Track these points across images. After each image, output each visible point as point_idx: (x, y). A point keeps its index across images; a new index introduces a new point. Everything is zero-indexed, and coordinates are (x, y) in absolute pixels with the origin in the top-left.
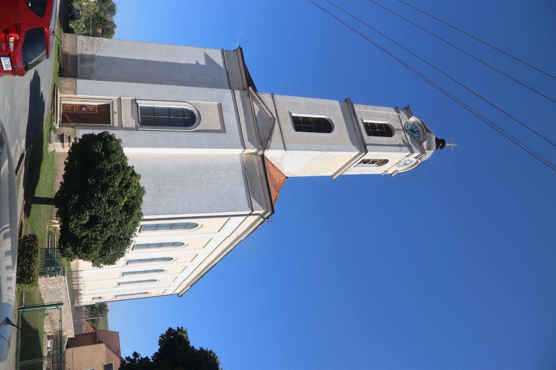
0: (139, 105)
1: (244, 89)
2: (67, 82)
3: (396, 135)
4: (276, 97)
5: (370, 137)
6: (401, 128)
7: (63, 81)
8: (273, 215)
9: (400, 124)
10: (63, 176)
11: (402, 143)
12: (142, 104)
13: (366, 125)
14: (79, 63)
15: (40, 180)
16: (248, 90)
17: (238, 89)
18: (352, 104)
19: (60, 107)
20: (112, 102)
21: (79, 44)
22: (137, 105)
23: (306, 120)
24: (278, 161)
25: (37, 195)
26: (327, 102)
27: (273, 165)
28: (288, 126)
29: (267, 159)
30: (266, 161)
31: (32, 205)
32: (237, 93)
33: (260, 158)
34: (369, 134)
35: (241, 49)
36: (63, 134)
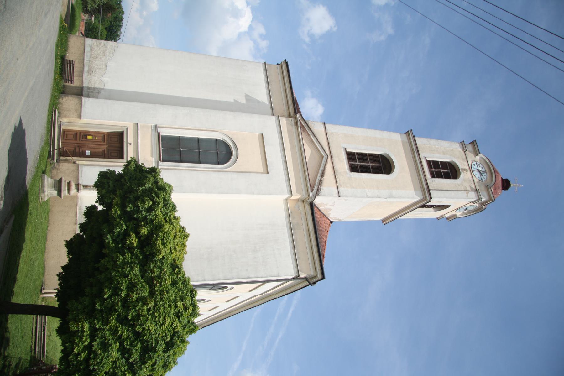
0: (161, 134)
1: (290, 116)
2: (68, 102)
3: (462, 175)
4: (327, 126)
5: (434, 179)
6: (467, 168)
7: (64, 99)
8: (323, 280)
9: (466, 163)
10: (59, 275)
11: (469, 189)
12: (165, 132)
13: (429, 162)
14: (85, 75)
15: (28, 151)
16: (296, 118)
17: (283, 116)
18: (414, 137)
19: (59, 135)
20: (127, 129)
21: (87, 49)
22: (159, 134)
23: (363, 157)
24: (327, 207)
25: (18, 299)
26: (385, 135)
27: (320, 210)
28: (343, 164)
29: (315, 205)
30: (315, 209)
31: (10, 316)
32: (284, 121)
33: (308, 207)
34: (433, 175)
35: (287, 63)
36: (61, 179)
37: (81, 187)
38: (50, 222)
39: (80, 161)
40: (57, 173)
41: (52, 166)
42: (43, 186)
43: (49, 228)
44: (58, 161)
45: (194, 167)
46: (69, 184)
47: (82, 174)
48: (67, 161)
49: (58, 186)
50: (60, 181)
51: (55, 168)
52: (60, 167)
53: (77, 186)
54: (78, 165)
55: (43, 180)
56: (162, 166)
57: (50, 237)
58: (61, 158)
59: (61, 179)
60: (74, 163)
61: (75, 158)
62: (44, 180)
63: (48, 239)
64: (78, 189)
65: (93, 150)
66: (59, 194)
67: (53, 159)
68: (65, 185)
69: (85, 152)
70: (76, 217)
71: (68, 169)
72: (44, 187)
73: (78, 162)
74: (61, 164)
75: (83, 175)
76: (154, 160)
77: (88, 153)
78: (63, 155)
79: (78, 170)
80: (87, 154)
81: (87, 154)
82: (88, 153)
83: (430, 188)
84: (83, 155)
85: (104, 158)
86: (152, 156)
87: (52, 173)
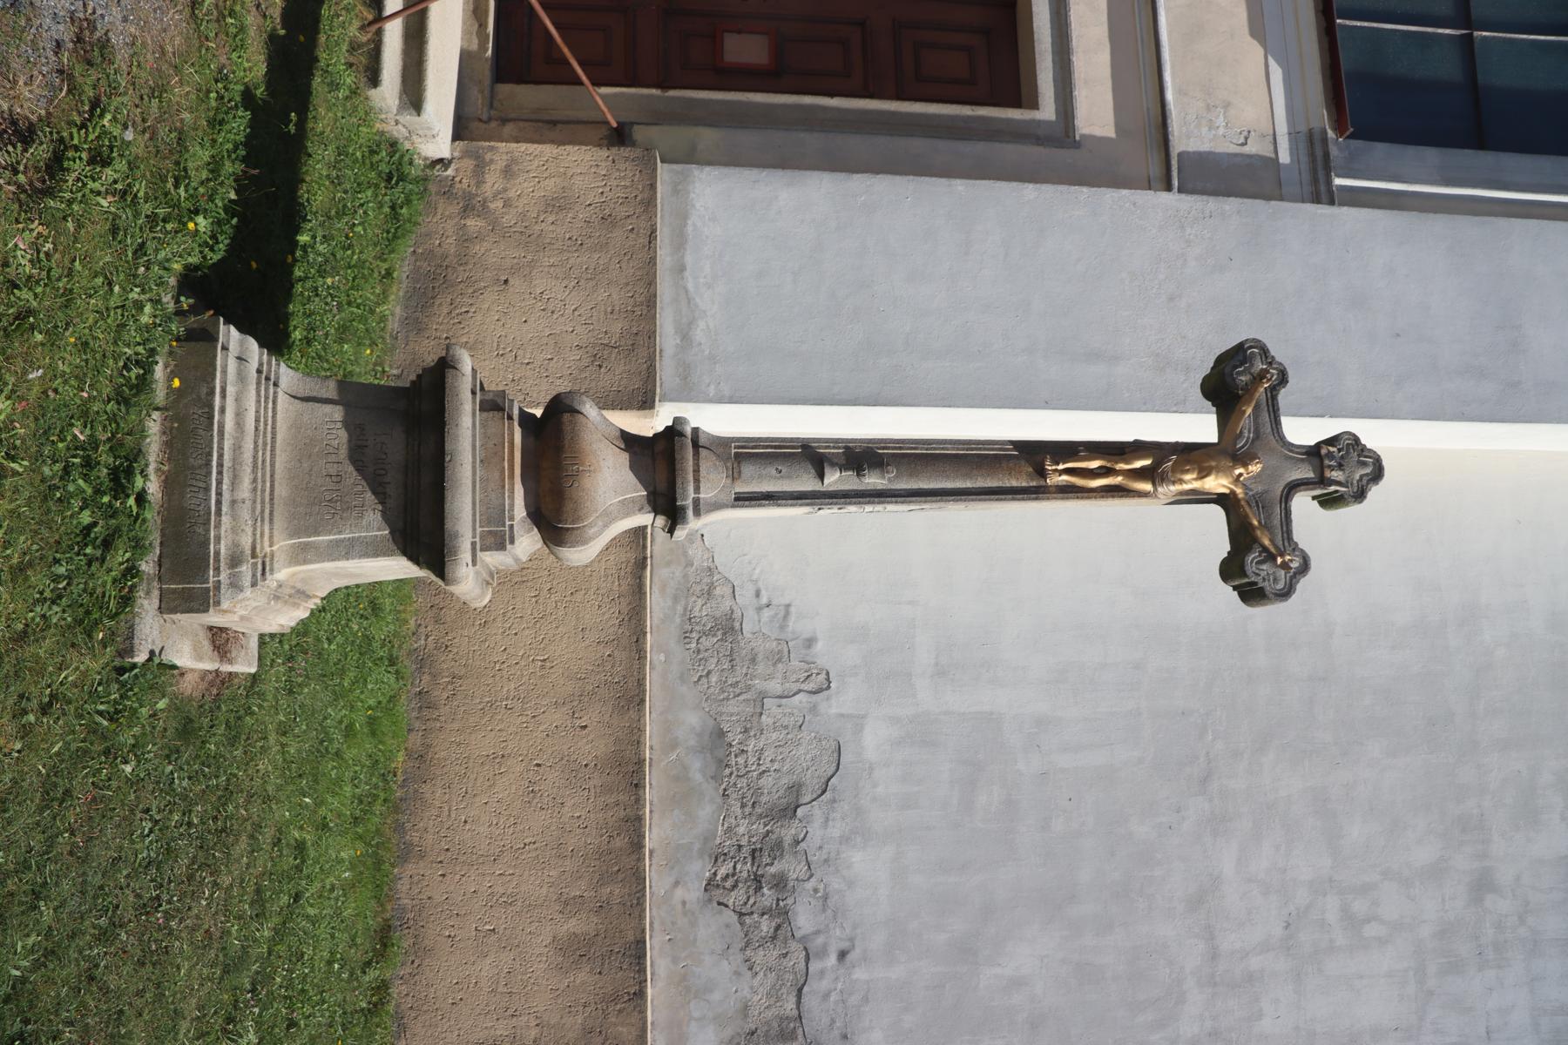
53: (662, 463)
68: (490, 457)
71: (557, 204)
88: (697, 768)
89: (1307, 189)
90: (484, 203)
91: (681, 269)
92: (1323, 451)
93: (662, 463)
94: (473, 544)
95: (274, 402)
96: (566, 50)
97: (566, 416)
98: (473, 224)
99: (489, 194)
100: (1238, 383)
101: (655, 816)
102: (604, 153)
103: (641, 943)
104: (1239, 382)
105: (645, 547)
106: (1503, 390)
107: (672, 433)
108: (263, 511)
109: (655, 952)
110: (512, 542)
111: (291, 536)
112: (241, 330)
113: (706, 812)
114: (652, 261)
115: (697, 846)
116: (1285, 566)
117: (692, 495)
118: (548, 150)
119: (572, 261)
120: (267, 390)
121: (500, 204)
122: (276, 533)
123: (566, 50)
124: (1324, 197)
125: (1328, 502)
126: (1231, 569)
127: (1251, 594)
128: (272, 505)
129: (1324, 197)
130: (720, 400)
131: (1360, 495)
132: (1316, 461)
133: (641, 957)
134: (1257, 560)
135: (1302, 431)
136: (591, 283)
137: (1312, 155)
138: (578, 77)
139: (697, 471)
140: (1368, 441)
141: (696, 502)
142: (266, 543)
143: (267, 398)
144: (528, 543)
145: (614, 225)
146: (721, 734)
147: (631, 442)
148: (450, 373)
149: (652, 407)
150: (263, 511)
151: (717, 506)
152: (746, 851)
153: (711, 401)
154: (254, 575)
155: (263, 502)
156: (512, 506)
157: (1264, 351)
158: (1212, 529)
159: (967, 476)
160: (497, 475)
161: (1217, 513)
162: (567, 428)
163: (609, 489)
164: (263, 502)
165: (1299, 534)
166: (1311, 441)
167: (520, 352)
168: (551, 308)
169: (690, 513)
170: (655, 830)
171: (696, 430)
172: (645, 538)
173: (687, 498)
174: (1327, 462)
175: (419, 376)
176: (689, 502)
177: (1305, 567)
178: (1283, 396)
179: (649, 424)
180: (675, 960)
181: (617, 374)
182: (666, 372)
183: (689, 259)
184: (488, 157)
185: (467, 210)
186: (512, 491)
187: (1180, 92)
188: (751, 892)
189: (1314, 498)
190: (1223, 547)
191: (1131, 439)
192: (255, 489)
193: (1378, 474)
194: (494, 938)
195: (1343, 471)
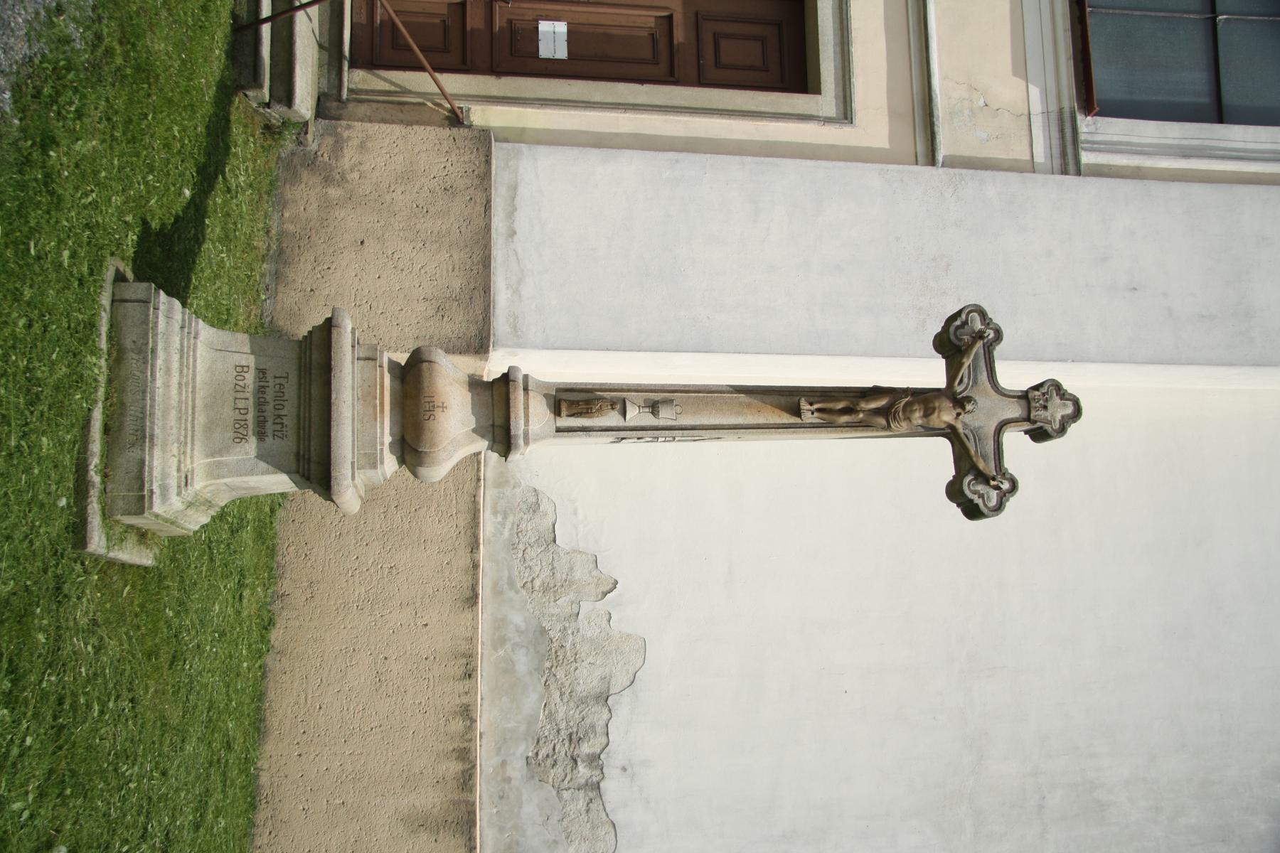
36: (328, 326)
37: (533, 416)
38: (285, 586)
39: (495, 106)
40: (327, 205)
41: (288, 144)
42: (127, 429)
43: (276, 636)
44: (330, 104)
45: (1186, 153)
46: (411, 380)
47: (511, 214)
48: (400, 109)
49: (295, 413)
50: (315, 356)
51: (311, 162)
52: (349, 157)
53: (497, 403)
54: (484, 139)
55: (129, 354)
56: (1096, 147)
57: (284, 705)
58: (356, 78)
59: (328, 326)
60: (455, 119)
61: (455, 83)
62: (145, 352)
63: (273, 721)
64: (502, 438)
65: (586, 13)
66: (316, 471)
67: (284, 93)
68: (368, 396)
69: (533, 35)
70: (474, 546)
71: (407, 176)
72: (142, 437)
73: (480, 116)
74: (355, 131)
75: (521, 223)
76: (1037, 107)
77: (553, 37)
78: (368, 58)
79: (484, 178)
80: (545, 51)
81: (545, 51)
82: (553, 37)
83: (1082, 137)
84: (512, 56)
85: (671, 77)
86: (1021, 69)
87: (282, 204)
88: (523, 662)
89: (1057, 163)
90: (343, 178)
91: (512, 233)
92: (1030, 395)
93: (497, 403)
94: (353, 463)
95: (194, 351)
96: (410, 40)
97: (425, 364)
98: (333, 192)
99: (347, 167)
100: (963, 341)
101: (486, 703)
102: (447, 132)
103: (472, 813)
104: (963, 341)
105: (478, 470)
106: (1243, 339)
107: (506, 379)
108: (186, 437)
109: (485, 824)
110: (382, 463)
111: (207, 456)
112: (169, 294)
113: (531, 701)
114: (488, 228)
115: (523, 728)
116: (997, 488)
117: (522, 427)
118: (397, 130)
119: (418, 226)
120: (189, 340)
121: (356, 175)
122: (196, 453)
123: (410, 40)
124: (1071, 167)
125: (1039, 435)
126: (954, 491)
127: (972, 512)
128: (193, 431)
129: (1071, 167)
130: (548, 346)
131: (1062, 430)
132: (1023, 402)
133: (472, 823)
134: (977, 486)
135: (1015, 374)
136: (435, 246)
137: (1062, 131)
138: (420, 62)
139: (526, 408)
140: (1068, 386)
141: (526, 435)
142: (188, 461)
143: (189, 347)
144: (390, 464)
145: (454, 195)
146: (543, 632)
147: (475, 384)
148: (334, 331)
149: (487, 351)
150: (186, 437)
151: (539, 438)
152: (564, 734)
153: (536, 347)
154: (179, 487)
155: (186, 429)
156: (382, 433)
157: (983, 314)
158: (937, 457)
159: (739, 414)
160: (371, 410)
161: (943, 447)
162: (426, 374)
163: (455, 424)
164: (186, 429)
165: (1010, 464)
166: (1024, 385)
167: (374, 304)
168: (401, 267)
169: (521, 442)
170: (484, 717)
171: (526, 377)
172: (479, 463)
173: (518, 427)
174: (1033, 404)
175: (310, 332)
176: (521, 432)
177: (1014, 486)
178: (998, 351)
179: (493, 367)
180: (502, 830)
181: (458, 324)
182: (500, 324)
183: (517, 226)
184: (346, 134)
185: (328, 180)
186: (382, 423)
187: (945, 78)
188: (569, 770)
189: (1026, 432)
190: (949, 472)
191: (871, 385)
192: (180, 418)
193: (1077, 413)
194: (343, 810)
195: (1046, 412)
